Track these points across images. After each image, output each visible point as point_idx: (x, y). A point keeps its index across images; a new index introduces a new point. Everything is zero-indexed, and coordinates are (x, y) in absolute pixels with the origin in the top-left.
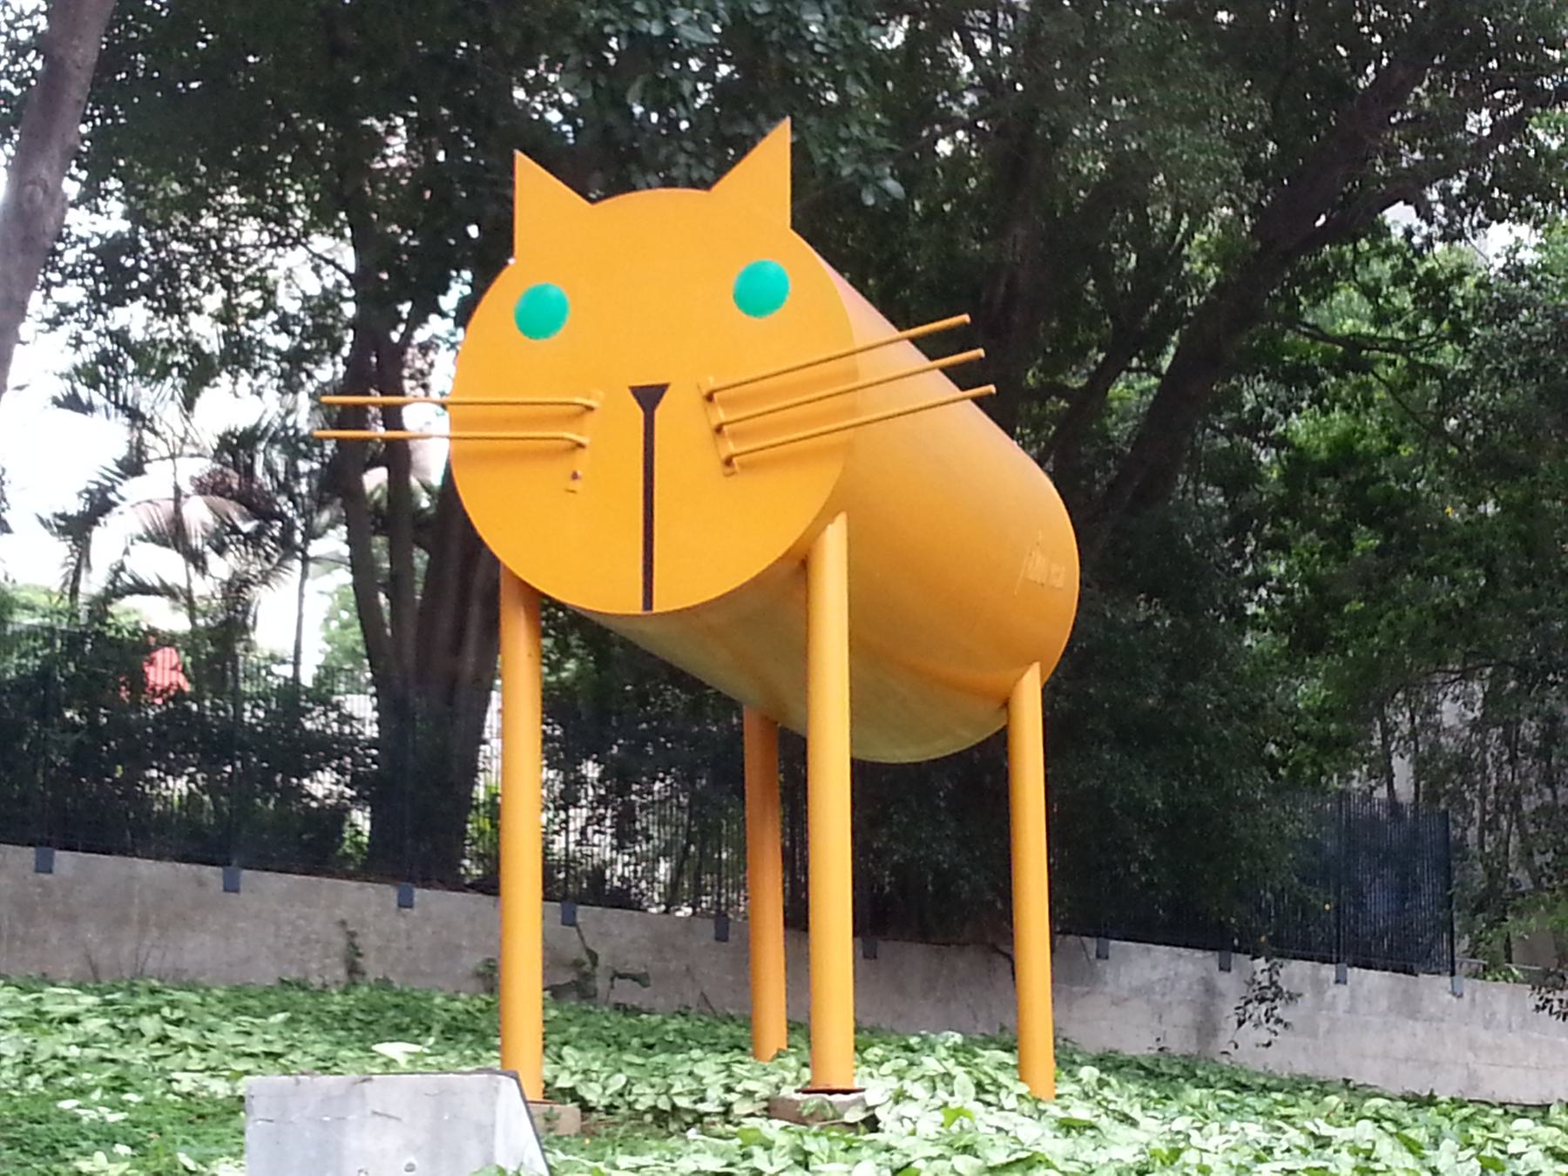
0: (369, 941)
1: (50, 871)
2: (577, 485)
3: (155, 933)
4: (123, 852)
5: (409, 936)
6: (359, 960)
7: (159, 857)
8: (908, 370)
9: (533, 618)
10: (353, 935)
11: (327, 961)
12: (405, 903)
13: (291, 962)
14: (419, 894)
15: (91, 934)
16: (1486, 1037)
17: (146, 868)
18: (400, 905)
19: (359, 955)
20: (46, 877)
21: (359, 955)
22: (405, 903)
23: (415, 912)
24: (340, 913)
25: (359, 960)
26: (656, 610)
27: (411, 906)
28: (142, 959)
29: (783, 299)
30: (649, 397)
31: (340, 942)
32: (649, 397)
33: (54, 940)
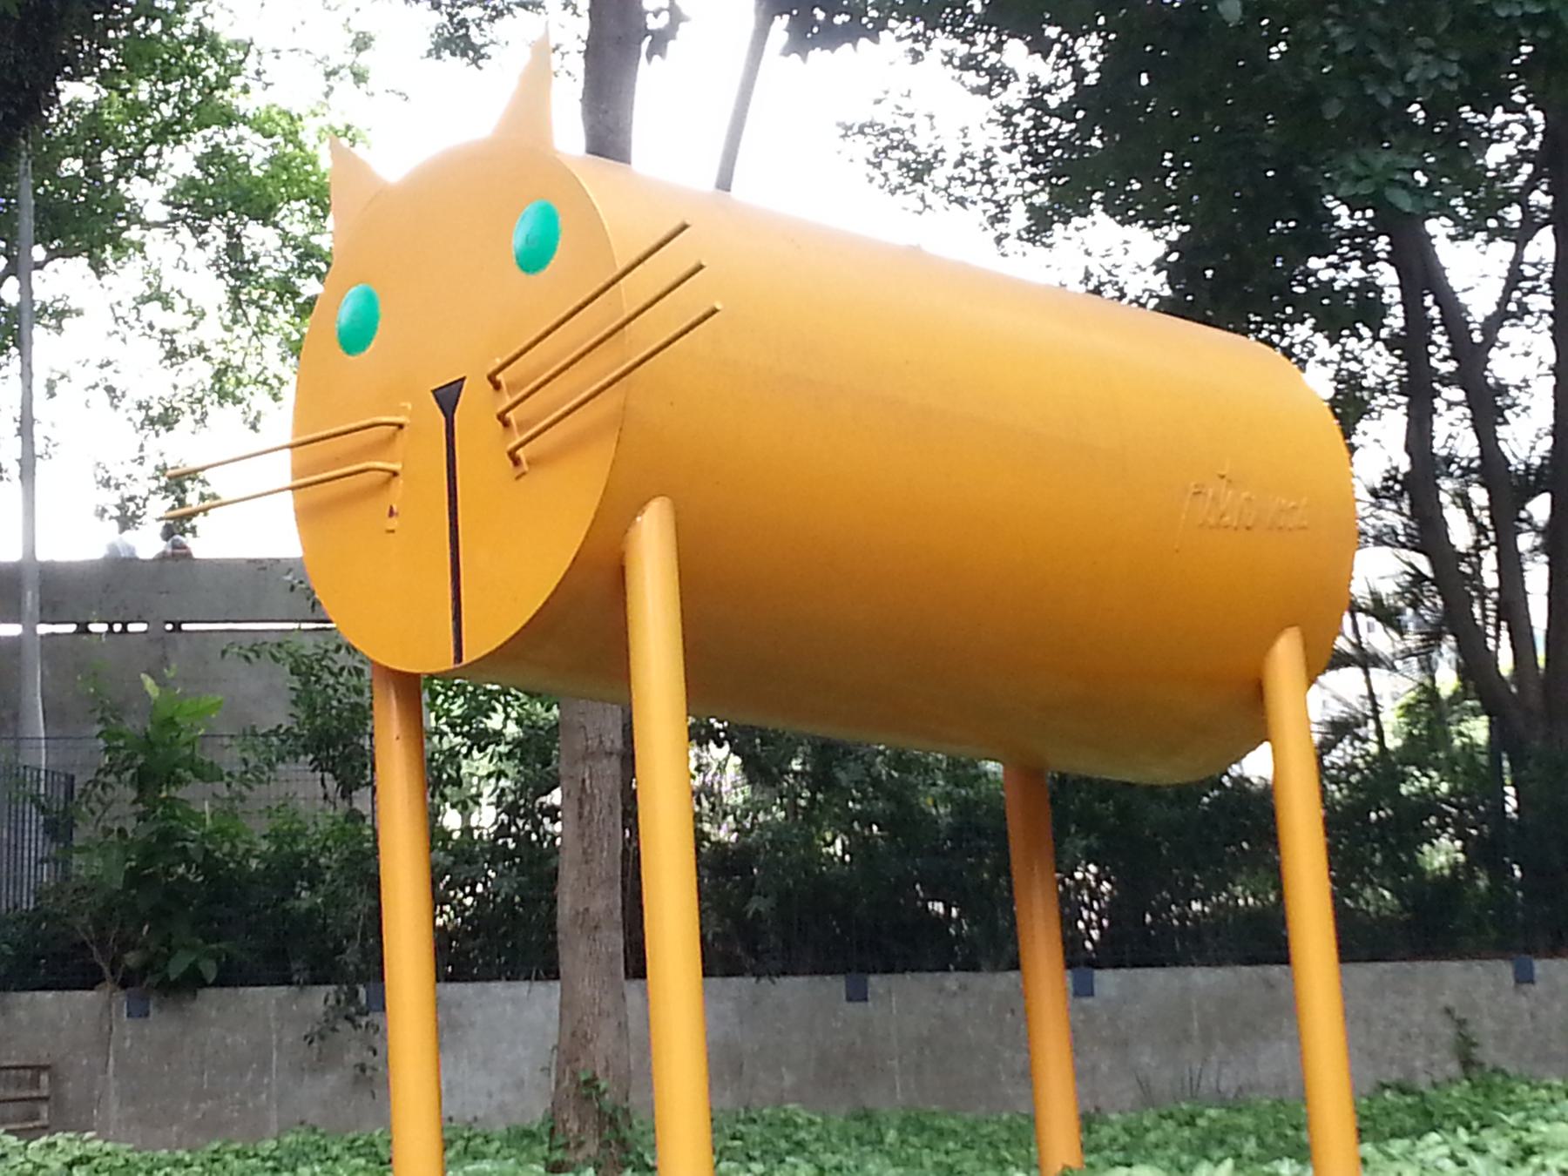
0: (1484, 1027)
1: (1091, 994)
2: (393, 523)
3: (1220, 1047)
4: (1177, 962)
5: (1533, 1016)
6: (1474, 1050)
7: (1220, 963)
8: (601, 285)
9: (1347, 655)
10: (1462, 1023)
11: (1436, 1056)
12: (1524, 977)
13: (1392, 1061)
14: (1540, 966)
15: (1146, 1058)
17: (1200, 977)
18: (1518, 981)
19: (1475, 1045)
20: (1087, 1001)
21: (1475, 1045)
22: (1524, 977)
23: (1538, 988)
24: (1447, 999)
25: (1474, 1050)
26: (465, 661)
27: (1531, 981)
28: (1195, 1078)
29: (554, 249)
30: (448, 398)
31: (1448, 1032)
32: (448, 398)
33: (1104, 1068)
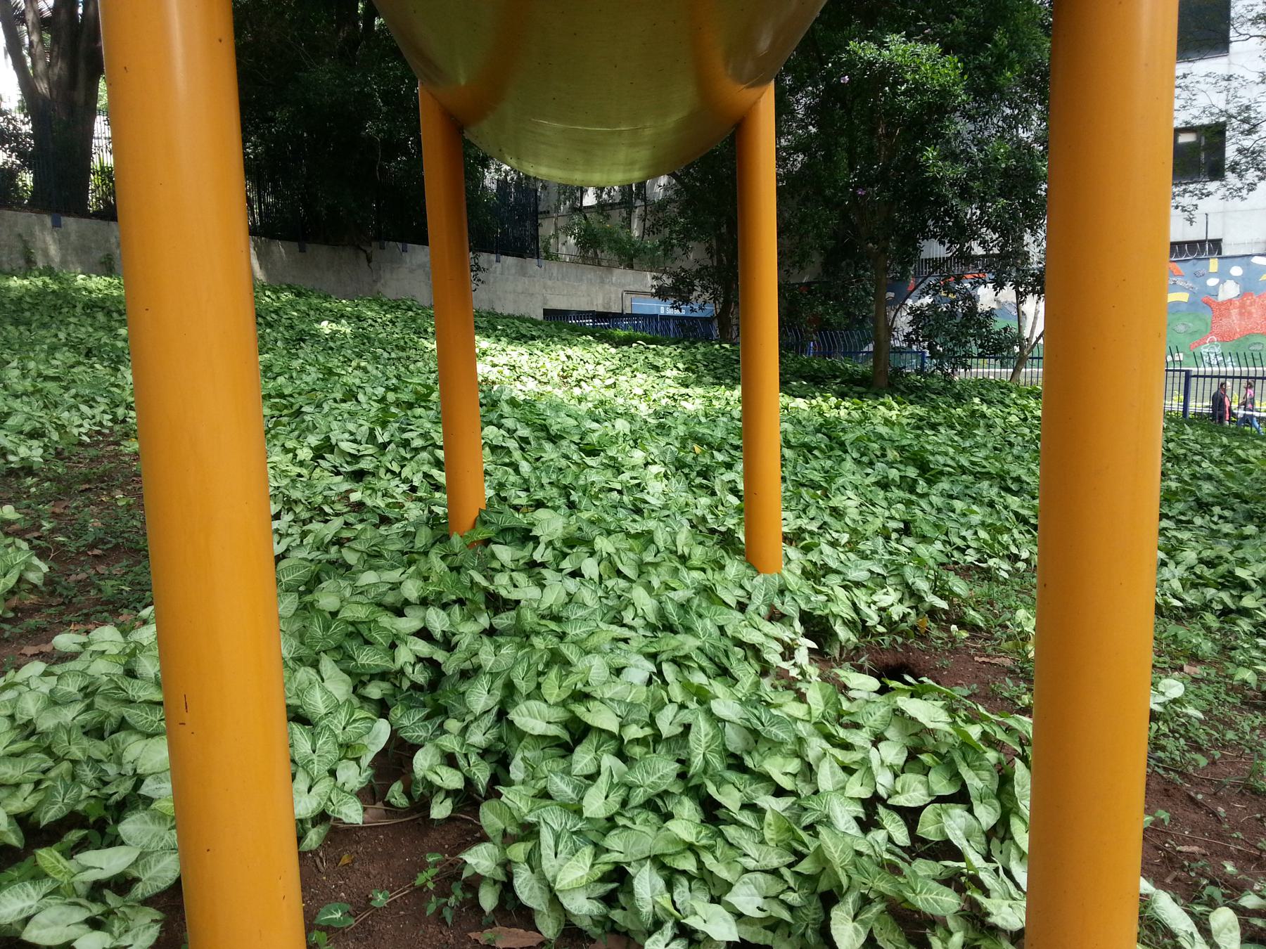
16: (550, 283)
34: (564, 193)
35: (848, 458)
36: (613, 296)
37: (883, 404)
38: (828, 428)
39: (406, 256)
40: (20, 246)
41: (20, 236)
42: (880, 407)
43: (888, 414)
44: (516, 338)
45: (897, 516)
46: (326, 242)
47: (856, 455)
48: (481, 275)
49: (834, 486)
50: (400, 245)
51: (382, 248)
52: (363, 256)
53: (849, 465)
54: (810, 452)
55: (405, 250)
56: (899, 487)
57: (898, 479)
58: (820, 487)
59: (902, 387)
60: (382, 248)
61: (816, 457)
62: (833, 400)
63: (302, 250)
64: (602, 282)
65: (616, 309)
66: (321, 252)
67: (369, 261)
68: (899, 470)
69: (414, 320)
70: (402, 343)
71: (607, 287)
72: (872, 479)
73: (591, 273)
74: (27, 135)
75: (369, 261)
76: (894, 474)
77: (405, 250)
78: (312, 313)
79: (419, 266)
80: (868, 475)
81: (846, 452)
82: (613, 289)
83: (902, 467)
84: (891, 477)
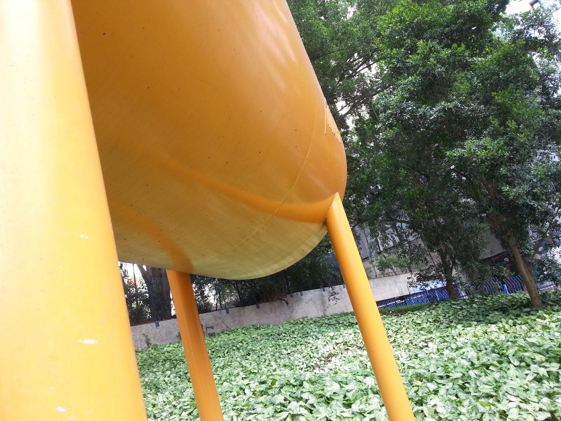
34: (371, 248)
35: (511, 366)
36: (403, 288)
37: (539, 317)
38: (499, 350)
39: (303, 297)
40: (144, 338)
41: (144, 334)
42: (538, 320)
43: (544, 322)
44: (349, 326)
45: (544, 408)
46: (268, 301)
47: (517, 363)
48: (337, 296)
49: (501, 393)
50: (299, 293)
51: (292, 296)
52: (284, 302)
53: (513, 372)
54: (488, 368)
55: (302, 295)
56: (548, 379)
57: (546, 374)
58: (492, 396)
59: (550, 303)
60: (292, 296)
61: (492, 371)
62: (511, 322)
63: (258, 307)
64: (396, 282)
65: (406, 293)
66: (265, 306)
67: (287, 304)
68: (546, 368)
69: (303, 328)
70: (294, 343)
71: (399, 284)
72: (530, 378)
73: (388, 281)
74: (146, 292)
75: (287, 304)
76: (543, 371)
77: (302, 295)
78: (259, 337)
79: (310, 300)
80: (527, 375)
81: (510, 362)
82: (402, 284)
83: (547, 364)
84: (541, 374)
